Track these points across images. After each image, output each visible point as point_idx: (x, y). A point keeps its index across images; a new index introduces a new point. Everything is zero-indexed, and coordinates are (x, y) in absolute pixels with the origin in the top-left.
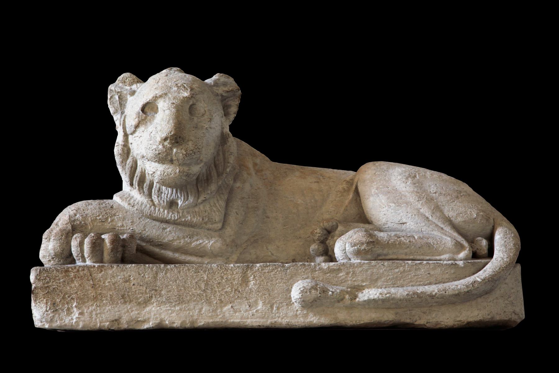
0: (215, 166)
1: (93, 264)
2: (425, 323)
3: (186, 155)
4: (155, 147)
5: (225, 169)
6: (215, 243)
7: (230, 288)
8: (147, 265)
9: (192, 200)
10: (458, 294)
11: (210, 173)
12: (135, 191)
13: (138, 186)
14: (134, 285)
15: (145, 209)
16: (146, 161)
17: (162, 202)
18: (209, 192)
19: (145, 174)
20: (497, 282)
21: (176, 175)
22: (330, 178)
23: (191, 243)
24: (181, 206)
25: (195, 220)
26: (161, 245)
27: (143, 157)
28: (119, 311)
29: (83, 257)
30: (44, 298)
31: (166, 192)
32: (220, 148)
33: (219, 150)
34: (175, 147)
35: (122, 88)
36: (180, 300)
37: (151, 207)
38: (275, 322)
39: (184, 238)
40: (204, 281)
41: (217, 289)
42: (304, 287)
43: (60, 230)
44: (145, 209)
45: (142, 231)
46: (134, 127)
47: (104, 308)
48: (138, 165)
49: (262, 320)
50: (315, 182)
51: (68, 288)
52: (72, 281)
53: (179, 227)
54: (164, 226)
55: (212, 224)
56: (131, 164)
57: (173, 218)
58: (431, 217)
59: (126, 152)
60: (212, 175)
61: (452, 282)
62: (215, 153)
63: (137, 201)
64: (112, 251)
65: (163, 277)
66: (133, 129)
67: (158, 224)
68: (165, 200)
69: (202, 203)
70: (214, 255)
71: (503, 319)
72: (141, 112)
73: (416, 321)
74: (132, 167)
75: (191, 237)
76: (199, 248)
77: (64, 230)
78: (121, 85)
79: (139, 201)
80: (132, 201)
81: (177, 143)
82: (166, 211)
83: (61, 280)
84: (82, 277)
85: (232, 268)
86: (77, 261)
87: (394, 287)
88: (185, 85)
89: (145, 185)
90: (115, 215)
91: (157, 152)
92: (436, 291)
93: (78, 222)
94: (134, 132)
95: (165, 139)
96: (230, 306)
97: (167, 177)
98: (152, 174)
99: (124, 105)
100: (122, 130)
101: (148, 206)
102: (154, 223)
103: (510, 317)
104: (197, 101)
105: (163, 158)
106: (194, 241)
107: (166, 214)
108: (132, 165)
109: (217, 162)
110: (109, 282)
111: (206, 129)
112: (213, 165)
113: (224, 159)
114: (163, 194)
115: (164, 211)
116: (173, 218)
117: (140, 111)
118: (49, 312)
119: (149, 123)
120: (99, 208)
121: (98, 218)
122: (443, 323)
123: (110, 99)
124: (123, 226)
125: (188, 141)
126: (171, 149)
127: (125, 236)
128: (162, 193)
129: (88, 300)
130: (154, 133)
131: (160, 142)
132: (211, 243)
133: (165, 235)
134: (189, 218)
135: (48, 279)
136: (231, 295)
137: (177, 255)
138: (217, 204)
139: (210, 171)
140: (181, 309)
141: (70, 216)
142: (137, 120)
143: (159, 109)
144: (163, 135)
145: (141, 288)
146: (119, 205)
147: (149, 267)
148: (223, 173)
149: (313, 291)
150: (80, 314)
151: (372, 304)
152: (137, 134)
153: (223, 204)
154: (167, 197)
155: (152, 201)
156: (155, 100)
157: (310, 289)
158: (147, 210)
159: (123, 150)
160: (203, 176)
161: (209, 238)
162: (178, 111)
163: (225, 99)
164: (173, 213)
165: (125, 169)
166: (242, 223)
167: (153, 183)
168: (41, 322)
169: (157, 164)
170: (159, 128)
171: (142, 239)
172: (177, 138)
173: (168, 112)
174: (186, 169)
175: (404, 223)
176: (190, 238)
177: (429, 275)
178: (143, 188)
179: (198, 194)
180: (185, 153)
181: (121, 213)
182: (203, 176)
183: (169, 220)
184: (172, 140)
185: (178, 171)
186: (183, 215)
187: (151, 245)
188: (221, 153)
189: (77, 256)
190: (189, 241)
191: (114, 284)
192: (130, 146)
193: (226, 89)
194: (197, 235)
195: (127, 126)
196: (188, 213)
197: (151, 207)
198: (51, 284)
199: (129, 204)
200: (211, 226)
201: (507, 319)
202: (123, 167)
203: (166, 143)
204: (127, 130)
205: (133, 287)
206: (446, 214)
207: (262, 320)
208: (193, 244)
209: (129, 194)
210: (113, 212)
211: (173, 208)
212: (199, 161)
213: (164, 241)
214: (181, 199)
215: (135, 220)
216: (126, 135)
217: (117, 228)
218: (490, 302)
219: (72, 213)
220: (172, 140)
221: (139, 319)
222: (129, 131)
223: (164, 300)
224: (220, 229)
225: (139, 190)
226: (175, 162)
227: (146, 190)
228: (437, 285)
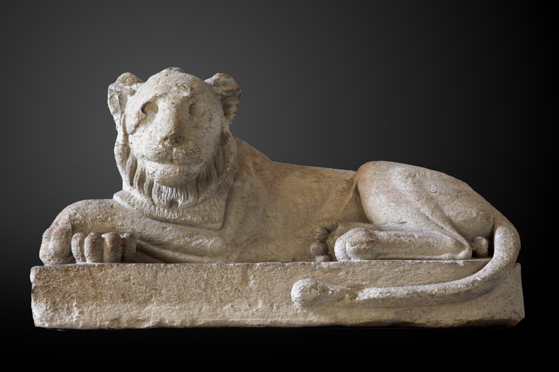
0: (215, 166)
1: (93, 263)
2: (425, 322)
3: (186, 155)
4: (155, 146)
5: (225, 168)
6: (215, 242)
7: (230, 288)
8: (147, 265)
9: (192, 200)
10: (458, 293)
11: (210, 173)
12: (135, 190)
13: (138, 185)
14: (134, 284)
15: (145, 209)
16: (146, 161)
17: (162, 201)
18: (209, 191)
19: (145, 173)
20: (497, 282)
21: (176, 175)
22: (330, 177)
23: (191, 242)
24: (181, 205)
25: (195, 219)
26: (161, 245)
27: (143, 157)
28: (119, 310)
29: (83, 256)
30: (44, 297)
31: (166, 192)
32: (220, 147)
33: (219, 150)
34: (175, 147)
35: (122, 88)
36: (180, 299)
37: (151, 206)
38: (275, 321)
39: (184, 237)
40: (204, 280)
41: (217, 289)
42: (304, 286)
43: (60, 229)
44: (145, 209)
45: (142, 230)
46: (134, 126)
47: (104, 307)
48: (138, 165)
49: (262, 320)
50: (315, 182)
51: (68, 287)
52: (72, 280)
53: (179, 227)
54: (164, 226)
55: (212, 223)
56: (131, 163)
57: (173, 218)
58: (431, 217)
59: (126, 151)
60: (212, 174)
61: (452, 281)
62: (215, 153)
63: (137, 200)
64: (112, 250)
65: (163, 276)
66: (133, 129)
67: (158, 223)
68: (165, 200)
69: (202, 202)
70: (214, 255)
71: (503, 318)
72: (141, 112)
73: (416, 321)
74: (132, 167)
75: (191, 236)
76: (199, 247)
77: (64, 229)
78: (121, 84)
79: (139, 200)
80: (132, 200)
81: (177, 142)
82: (166, 211)
83: (61, 280)
84: (82, 276)
85: (232, 267)
86: (77, 261)
87: (394, 286)
88: (185, 85)
89: (145, 184)
90: (115, 214)
91: (157, 152)
92: (436, 290)
93: (78, 222)
94: (134, 132)
95: (165, 139)
96: (230, 305)
97: (167, 177)
98: (152, 174)
99: (124, 105)
100: (122, 130)
101: (148, 205)
102: (154, 222)
103: (510, 316)
104: (197, 100)
105: (163, 157)
106: (194, 241)
107: (166, 214)
108: (132, 164)
109: (217, 162)
110: (109, 281)
111: (206, 128)
112: (213, 165)
113: (224, 158)
114: (163, 194)
115: (164, 210)
116: (173, 218)
117: (140, 111)
118: (49, 311)
119: (149, 123)
120: (99, 208)
121: (98, 217)
122: (443, 322)
123: (110, 99)
124: (123, 225)
125: (188, 140)
126: (171, 148)
127: (125, 236)
128: (162, 192)
129: (88, 300)
130: (154, 132)
131: (160, 142)
132: (211, 243)
133: (165, 234)
134: (189, 217)
135: (48, 278)
136: (231, 295)
137: (177, 255)
138: (217, 204)
139: (210, 170)
140: (181, 309)
141: (70, 215)
142: (137, 119)
143: (159, 109)
144: (163, 135)
145: (141, 287)
146: (119, 204)
147: (149, 266)
148: (223, 173)
149: (313, 291)
150: (80, 313)
151: (372, 303)
152: (137, 133)
153: (223, 203)
154: (167, 196)
155: (152, 200)
156: (155, 100)
157: (310, 288)
158: (147, 210)
159: (123, 149)
160: (203, 175)
161: (209, 237)
162: (178, 111)
163: (225, 99)
164: (173, 213)
165: (125, 169)
166: (242, 223)
167: (153, 183)
168: (41, 321)
169: (157, 164)
170: (159, 128)
171: (142, 238)
172: (177, 137)
173: (168, 112)
174: (186, 168)
175: (404, 223)
176: (190, 237)
177: (429, 275)
178: (143, 188)
179: (198, 193)
180: (185, 152)
181: (121, 213)
182: (203, 175)
183: (169, 219)
184: (172, 139)
185: (178, 170)
186: (183, 215)
187: (151, 244)
188: (221, 153)
189: (77, 256)
190: (189, 240)
191: (114, 283)
192: (130, 145)
193: (226, 89)
194: (197, 235)
195: (127, 126)
196: (188, 212)
197: (151, 206)
198: (51, 283)
199: (129, 203)
200: (211, 225)
201: (507, 318)
202: (123, 166)
203: (166, 143)
204: (127, 129)
205: (133, 286)
206: (446, 213)
207: (262, 320)
208: (193, 244)
209: (129, 194)
210: (113, 212)
211: (173, 207)
212: (199, 161)
213: (164, 240)
214: (181, 198)
215: (135, 220)
216: (126, 135)
217: (117, 228)
218: (490, 301)
219: (72, 212)
220: (172, 139)
221: (139, 318)
222: (129, 131)
223: (164, 299)
224: (220, 229)
225: (139, 189)
226: (175, 162)
227: (146, 189)
228: (437, 284)
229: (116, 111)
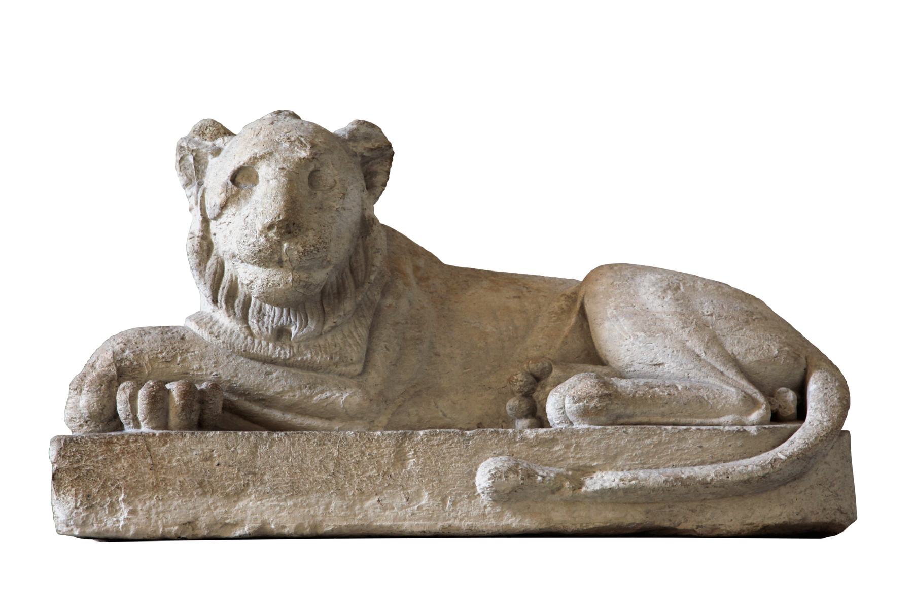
0: (352, 271)
1: (151, 431)
2: (694, 527)
3: (303, 253)
4: (253, 240)
5: (367, 276)
6: (350, 396)
7: (375, 471)
8: (240, 433)
9: (313, 327)
10: (748, 480)
11: (344, 283)
12: (220, 311)
13: (226, 303)
14: (218, 465)
15: (237, 342)
16: (238, 263)
17: (264, 330)
18: (342, 313)
19: (236, 284)
20: (812, 461)
21: (288, 286)
23: (312, 397)
24: (296, 336)
25: (318, 359)
26: (264, 401)
27: (234, 256)
28: (195, 508)
29: (135, 419)
30: (72, 487)
31: (272, 314)
32: (360, 241)
33: (357, 245)
34: (286, 240)
35: (200, 144)
37: (246, 338)
38: (450, 526)
39: (300, 388)
40: (333, 459)
41: (354, 473)
42: (496, 468)
43: (98, 375)
44: (237, 342)
45: (233, 377)
46: (218, 207)
47: (170, 502)
48: (226, 269)
49: (428, 523)
50: (515, 297)
51: (111, 470)
52: (118, 459)
53: (293, 371)
54: (268, 369)
55: (346, 366)
56: (214, 267)
57: (282, 357)
58: (703, 355)
59: (205, 248)
60: (347, 285)
61: (738, 460)
62: (352, 250)
63: (224, 328)
64: (183, 410)
65: (266, 452)
66: (217, 211)
67: (257, 365)
68: (270, 327)
69: (329, 331)
70: (349, 417)
71: (821, 520)
72: (231, 184)
73: (679, 525)
74: (215, 273)
75: (312, 386)
76: (325, 404)
77: (105, 375)
78: (197, 138)
79: (227, 328)
80: (216, 327)
81: (289, 233)
82: (271, 345)
83: (100, 458)
84: (133, 452)
85: (379, 437)
86: (126, 427)
87: (643, 468)
88: (302, 139)
89: (237, 302)
90: (187, 351)
91: (257, 248)
92: (713, 475)
93: (128, 363)
94: (219, 215)
95: (270, 227)
96: (376, 499)
97: (273, 289)
98: (248, 285)
99: (203, 172)
100: (200, 213)
101: (242, 336)
102: (252, 364)
103: (833, 517)
104: (322, 164)
105: (266, 257)
106: (317, 394)
107: (271, 350)
108: (216, 269)
109: (355, 265)
110: (178, 461)
111: (337, 210)
112: (347, 270)
113: (367, 259)
114: (266, 317)
115: (268, 344)
116: (282, 357)
117: (229, 182)
118: (81, 509)
119: (243, 201)
120: (162, 340)
121: (160, 356)
122: (723, 528)
124: (200, 368)
125: (307, 230)
126: (280, 243)
127: (204, 386)
128: (264, 315)
129: (144, 490)
130: (251, 217)
131: (262, 232)
132: (344, 397)
133: (269, 383)
134: (309, 356)
135: (79, 455)
136: (378, 482)
137: (289, 417)
138: (354, 334)
139: (342, 279)
140: (295, 505)
141: (114, 353)
142: (223, 195)
143: (260, 179)
144: (266, 221)
145: (231, 470)
146: (195, 334)
147: (243, 436)
148: (363, 283)
149: (512, 476)
150: (131, 512)
151: (607, 496)
152: (224, 218)
153: (364, 333)
154: (273, 322)
155: (248, 328)
156: (253, 164)
157: (507, 472)
158: (240, 343)
159: (201, 245)
160: (332, 287)
161: (341, 388)
162: (290, 181)
163: (368, 162)
164: (282, 348)
165: (204, 276)
166: (395, 365)
167: (250, 299)
168: (68, 526)
169: (256, 268)
170: (260, 209)
171: (232, 390)
172: (289, 225)
173: (274, 183)
174: (304, 275)
175: (659, 365)
176: (310, 388)
177: (700, 449)
178: (233, 308)
179: (323, 316)
180: (302, 250)
181: (197, 348)
182: (332, 287)
183: (275, 359)
184: (281, 228)
185: (290, 279)
186: (298, 351)
187: (246, 400)
188: (361, 250)
189: (126, 419)
190: (308, 394)
191: (186, 464)
192: (213, 238)
193: (369, 145)
194: (322, 384)
195: (207, 205)
196: (307, 347)
197: (246, 338)
198: (83, 463)
199: (211, 333)
200: (344, 369)
201: (828, 520)
202: (200, 272)
203: (271, 234)
204: (208, 212)
205: (217, 469)
206: (729, 349)
207: (428, 523)
208: (316, 399)
209: (211, 317)
210: (185, 347)
211: (283, 339)
212: (325, 263)
213: (268, 394)
214: (295, 325)
215: (220, 360)
217: (192, 372)
218: (801, 492)
220: (281, 228)
221: (227, 521)
222: (210, 214)
223: (268, 489)
224: (360, 374)
225: (227, 310)
226: (285, 264)
227: (238, 310)
228: (714, 466)
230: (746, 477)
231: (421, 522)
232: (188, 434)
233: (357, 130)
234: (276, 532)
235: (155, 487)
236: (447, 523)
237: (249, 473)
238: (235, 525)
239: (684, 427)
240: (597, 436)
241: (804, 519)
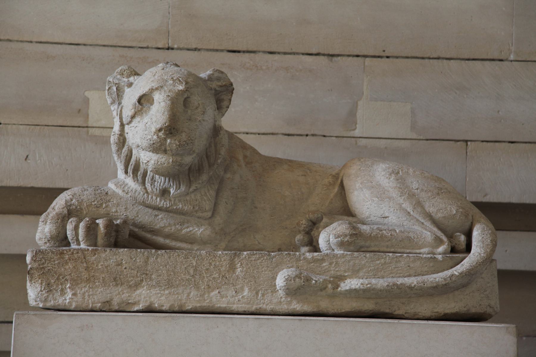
0: (207, 157)
2: (404, 313)
6: (204, 230)
7: (217, 275)
8: (139, 250)
9: (183, 189)
12: (129, 178)
13: (133, 174)
14: (125, 268)
15: (139, 196)
17: (155, 190)
19: (139, 163)
23: (181, 230)
25: (186, 208)
27: (138, 146)
28: (111, 293)
30: (39, 279)
34: (169, 138)
35: (120, 80)
37: (144, 194)
38: (260, 308)
39: (175, 225)
40: (193, 267)
42: (288, 275)
43: (57, 214)
44: (139, 196)
45: (135, 217)
47: (96, 289)
51: (63, 269)
52: (67, 263)
53: (171, 214)
54: (156, 213)
55: (202, 213)
56: (126, 152)
57: (165, 206)
59: (122, 141)
63: (131, 188)
64: (105, 235)
65: (154, 262)
66: (129, 119)
68: (158, 189)
69: (193, 192)
70: (203, 242)
73: (395, 311)
74: (127, 156)
75: (182, 224)
76: (189, 235)
77: (61, 214)
78: (119, 76)
80: (126, 188)
81: (171, 133)
82: (158, 199)
84: (76, 259)
85: (220, 255)
86: (72, 244)
87: (374, 278)
89: (139, 173)
90: (109, 201)
91: (152, 142)
92: (415, 283)
93: (74, 207)
94: (130, 122)
95: (160, 130)
97: (161, 166)
98: (146, 163)
99: (122, 96)
101: (142, 193)
102: (147, 210)
103: (485, 309)
105: (157, 148)
106: (184, 229)
107: (159, 202)
108: (128, 153)
110: (102, 265)
111: (200, 121)
112: (204, 156)
114: (156, 183)
116: (165, 206)
118: (44, 292)
119: (144, 114)
120: (95, 194)
122: (420, 314)
123: (108, 90)
124: (116, 212)
125: (182, 132)
126: (165, 139)
127: (118, 222)
128: (155, 181)
130: (149, 123)
131: (155, 133)
132: (201, 231)
134: (181, 206)
135: (44, 260)
136: (219, 281)
137: (168, 241)
138: (208, 194)
140: (170, 293)
142: (133, 110)
143: (155, 101)
144: (158, 126)
145: (133, 271)
146: (114, 191)
147: (141, 252)
148: (214, 164)
149: (297, 280)
152: (132, 124)
153: (213, 193)
154: (160, 185)
155: (145, 188)
156: (151, 92)
157: (294, 278)
158: (141, 196)
159: (119, 139)
166: (231, 213)
167: (147, 172)
168: (36, 301)
169: (151, 153)
170: (154, 119)
171: (135, 225)
172: (171, 129)
173: (163, 104)
174: (179, 159)
175: (386, 217)
176: (181, 225)
178: (137, 176)
179: (190, 183)
183: (161, 207)
185: (171, 160)
187: (143, 231)
188: (213, 145)
189: (72, 240)
191: (106, 267)
192: (126, 135)
193: (219, 84)
194: (187, 223)
196: (180, 201)
197: (144, 194)
198: (46, 265)
199: (123, 191)
201: (482, 312)
202: (118, 155)
203: (161, 134)
204: (124, 120)
206: (427, 209)
207: (248, 306)
209: (124, 182)
210: (108, 199)
213: (156, 227)
215: (128, 207)
216: (122, 125)
217: (111, 214)
219: (68, 198)
220: (166, 131)
221: (130, 301)
222: (125, 121)
223: (154, 283)
224: (210, 218)
225: (133, 178)
226: (168, 152)
227: (140, 178)
228: (416, 277)
229: (113, 102)
230: (435, 285)
231: (243, 305)
232: (108, 250)
233: (213, 74)
234: (158, 309)
235: (88, 280)
236: (258, 307)
237: (143, 274)
238: (134, 304)
239: (400, 255)
240: (348, 258)
241: (468, 310)
